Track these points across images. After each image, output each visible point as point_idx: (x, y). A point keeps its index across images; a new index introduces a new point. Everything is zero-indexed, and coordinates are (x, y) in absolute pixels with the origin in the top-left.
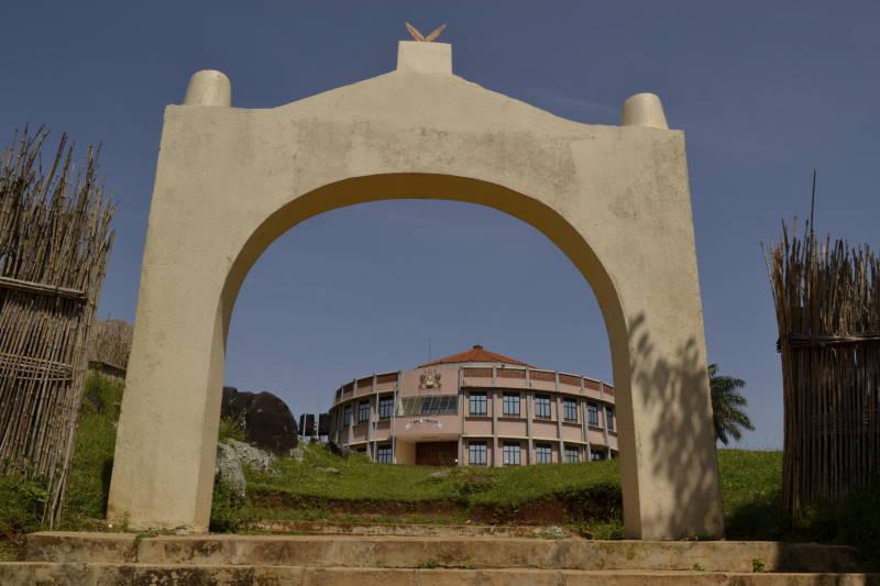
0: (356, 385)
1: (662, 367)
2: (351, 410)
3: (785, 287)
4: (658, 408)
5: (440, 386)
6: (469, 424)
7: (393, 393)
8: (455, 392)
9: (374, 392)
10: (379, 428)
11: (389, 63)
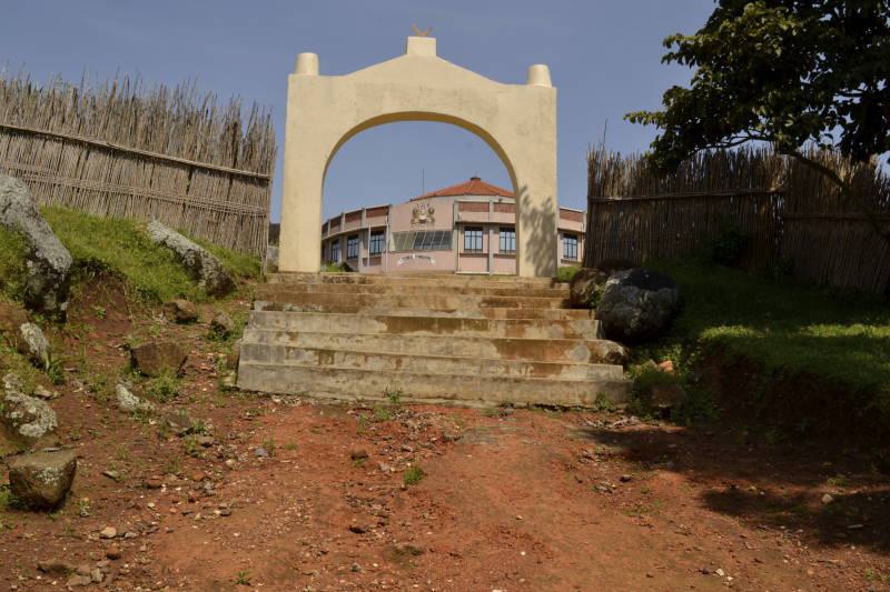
0: (344, 219)
1: (534, 212)
2: (338, 245)
3: (593, 166)
4: (530, 231)
5: (433, 220)
6: (463, 261)
7: (385, 227)
8: (450, 228)
9: (364, 227)
10: (371, 264)
11: (402, 50)
